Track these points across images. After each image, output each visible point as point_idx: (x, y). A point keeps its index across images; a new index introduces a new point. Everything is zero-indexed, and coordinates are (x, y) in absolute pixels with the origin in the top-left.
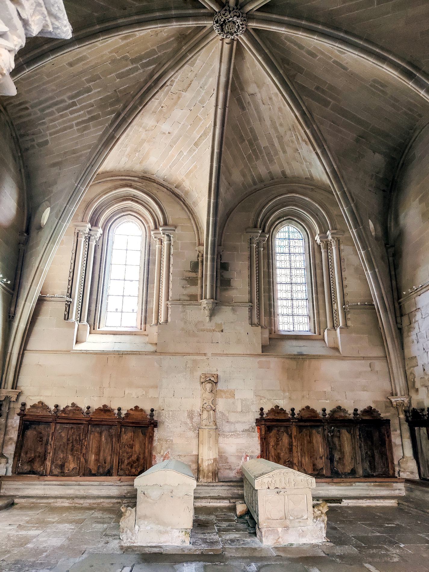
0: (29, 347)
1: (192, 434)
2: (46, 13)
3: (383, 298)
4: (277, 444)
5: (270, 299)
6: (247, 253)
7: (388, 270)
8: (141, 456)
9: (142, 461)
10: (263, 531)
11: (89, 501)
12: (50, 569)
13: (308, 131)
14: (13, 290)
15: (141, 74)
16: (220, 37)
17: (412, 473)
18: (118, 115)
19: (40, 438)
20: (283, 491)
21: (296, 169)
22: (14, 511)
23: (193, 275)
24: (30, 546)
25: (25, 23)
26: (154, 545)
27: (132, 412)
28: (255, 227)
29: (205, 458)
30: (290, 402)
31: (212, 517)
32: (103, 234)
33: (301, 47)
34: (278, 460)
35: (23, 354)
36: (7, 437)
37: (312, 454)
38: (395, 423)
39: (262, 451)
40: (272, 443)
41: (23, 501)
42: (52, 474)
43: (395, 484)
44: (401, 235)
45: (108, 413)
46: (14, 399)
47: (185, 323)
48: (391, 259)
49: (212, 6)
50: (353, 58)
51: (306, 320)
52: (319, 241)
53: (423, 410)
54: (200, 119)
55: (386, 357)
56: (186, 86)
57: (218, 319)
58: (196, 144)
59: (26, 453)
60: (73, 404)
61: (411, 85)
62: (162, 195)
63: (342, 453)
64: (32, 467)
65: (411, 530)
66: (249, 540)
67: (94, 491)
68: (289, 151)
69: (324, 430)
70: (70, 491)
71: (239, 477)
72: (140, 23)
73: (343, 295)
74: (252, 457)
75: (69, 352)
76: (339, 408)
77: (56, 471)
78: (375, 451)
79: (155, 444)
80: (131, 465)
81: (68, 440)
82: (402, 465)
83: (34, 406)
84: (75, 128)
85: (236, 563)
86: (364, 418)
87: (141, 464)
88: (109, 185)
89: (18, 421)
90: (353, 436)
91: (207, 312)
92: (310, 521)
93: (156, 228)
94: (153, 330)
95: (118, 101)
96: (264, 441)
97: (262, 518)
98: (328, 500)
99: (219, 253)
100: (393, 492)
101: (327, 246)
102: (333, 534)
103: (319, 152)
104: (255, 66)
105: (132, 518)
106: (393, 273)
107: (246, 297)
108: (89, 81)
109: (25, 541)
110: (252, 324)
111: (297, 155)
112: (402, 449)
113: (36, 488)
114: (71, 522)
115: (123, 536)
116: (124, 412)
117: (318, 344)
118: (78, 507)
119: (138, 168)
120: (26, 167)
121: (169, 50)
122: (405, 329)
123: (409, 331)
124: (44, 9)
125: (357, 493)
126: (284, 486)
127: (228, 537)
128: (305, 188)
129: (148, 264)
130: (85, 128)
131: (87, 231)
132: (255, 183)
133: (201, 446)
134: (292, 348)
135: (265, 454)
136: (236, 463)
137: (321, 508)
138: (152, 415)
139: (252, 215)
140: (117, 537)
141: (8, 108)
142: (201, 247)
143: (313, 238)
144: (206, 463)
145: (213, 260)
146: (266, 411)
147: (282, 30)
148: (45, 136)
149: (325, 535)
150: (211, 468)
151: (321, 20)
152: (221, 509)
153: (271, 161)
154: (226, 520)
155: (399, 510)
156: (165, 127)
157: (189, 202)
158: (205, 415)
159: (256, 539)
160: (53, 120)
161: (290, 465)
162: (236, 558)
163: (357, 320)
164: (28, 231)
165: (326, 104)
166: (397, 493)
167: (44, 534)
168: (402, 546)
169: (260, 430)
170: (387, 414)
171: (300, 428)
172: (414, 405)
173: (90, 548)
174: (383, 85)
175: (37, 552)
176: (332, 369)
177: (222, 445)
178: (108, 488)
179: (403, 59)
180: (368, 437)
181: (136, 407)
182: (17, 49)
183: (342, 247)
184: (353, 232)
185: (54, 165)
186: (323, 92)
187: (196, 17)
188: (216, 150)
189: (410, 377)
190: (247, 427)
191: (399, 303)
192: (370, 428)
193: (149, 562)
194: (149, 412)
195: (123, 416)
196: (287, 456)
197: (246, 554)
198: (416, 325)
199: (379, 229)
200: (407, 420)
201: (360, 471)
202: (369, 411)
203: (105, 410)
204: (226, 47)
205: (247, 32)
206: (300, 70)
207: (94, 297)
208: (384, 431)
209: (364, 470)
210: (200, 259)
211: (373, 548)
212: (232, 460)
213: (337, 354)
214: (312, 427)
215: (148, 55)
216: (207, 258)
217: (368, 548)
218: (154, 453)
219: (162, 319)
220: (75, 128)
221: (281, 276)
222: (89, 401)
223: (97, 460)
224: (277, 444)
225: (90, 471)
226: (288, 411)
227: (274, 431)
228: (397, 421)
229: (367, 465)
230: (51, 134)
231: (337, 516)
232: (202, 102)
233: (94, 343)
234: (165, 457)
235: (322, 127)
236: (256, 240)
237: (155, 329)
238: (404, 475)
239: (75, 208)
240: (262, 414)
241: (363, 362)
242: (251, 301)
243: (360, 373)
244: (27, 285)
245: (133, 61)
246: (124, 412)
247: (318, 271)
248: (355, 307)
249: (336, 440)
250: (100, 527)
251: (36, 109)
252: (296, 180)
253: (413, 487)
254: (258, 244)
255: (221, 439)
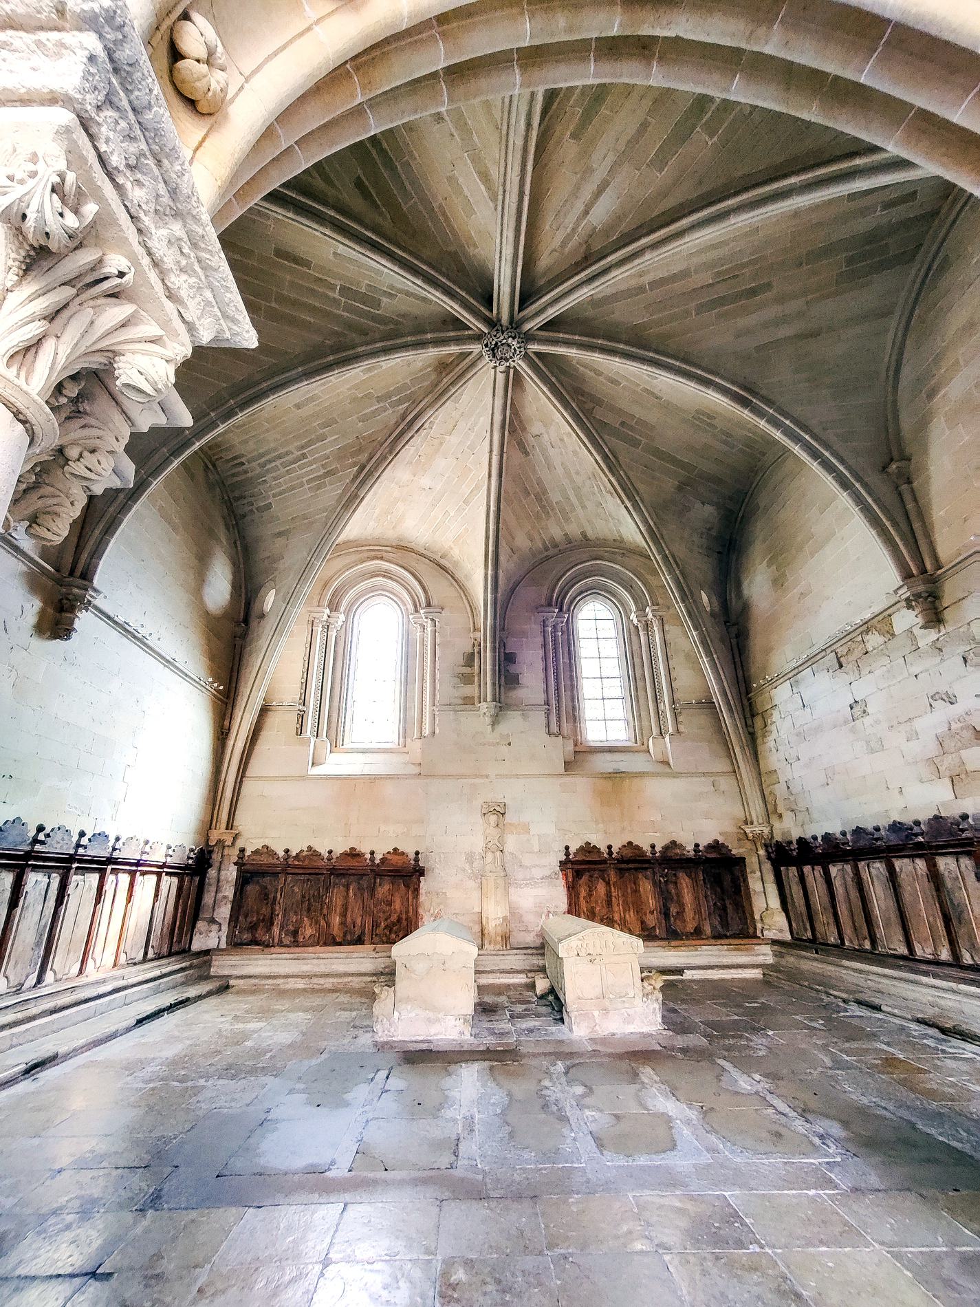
0: (247, 774)
1: (471, 884)
2: (219, 314)
3: (724, 691)
4: (590, 895)
5: (573, 700)
6: (540, 640)
7: (730, 657)
8: (404, 916)
9: (405, 923)
10: (573, 1015)
11: (331, 980)
12: (276, 1076)
13: (613, 479)
14: (228, 697)
15: (390, 415)
16: (492, 364)
17: (781, 931)
18: (363, 468)
19: (265, 896)
20: (598, 958)
21: (600, 528)
22: (228, 997)
23: (468, 670)
24: (249, 1044)
25: (191, 328)
26: (421, 1038)
27: (389, 857)
28: (550, 604)
29: (492, 916)
30: (607, 837)
31: (503, 999)
32: (346, 622)
33: (599, 373)
34: (592, 916)
35: (241, 782)
36: (220, 895)
37: (639, 908)
38: (752, 862)
39: (570, 905)
40: (583, 894)
41: (241, 982)
42: (281, 944)
43: (757, 947)
44: (745, 608)
45: (358, 859)
46: (229, 843)
47: (458, 735)
48: (734, 641)
49: (480, 326)
50: (667, 384)
51: (622, 725)
52: (635, 621)
53: (790, 843)
54: (470, 470)
55: (735, 772)
56: (451, 427)
57: (503, 728)
58: (466, 502)
59: (246, 917)
60: (310, 848)
61: (746, 414)
62: (423, 568)
63: (681, 905)
64: (253, 936)
65: (783, 1012)
66: (553, 1029)
67: (340, 967)
68: (589, 505)
69: (654, 874)
70: (305, 967)
71: (538, 942)
72: (386, 351)
73: (672, 691)
74: (555, 913)
75: (303, 778)
76: (674, 842)
77: (287, 940)
78: (727, 902)
79: (422, 898)
80: (390, 928)
81: (303, 897)
82: (766, 921)
83: (256, 852)
84: (306, 487)
85: (534, 1062)
86: (709, 856)
87: (403, 926)
88: (354, 558)
89: (235, 873)
90: (695, 880)
91: (488, 720)
92: (638, 1001)
93: (417, 611)
94: (416, 746)
95: (360, 450)
96: (572, 889)
97: (570, 997)
98: (664, 971)
99: (501, 640)
100: (755, 958)
101: (647, 626)
102: (674, 1021)
103: (629, 505)
104: (540, 402)
105: (390, 1002)
106: (737, 660)
107: (541, 698)
108: (325, 425)
109: (245, 1036)
110: (549, 734)
111: (600, 510)
112: (764, 898)
113: (258, 964)
114: (305, 1011)
115: (378, 1028)
116: (378, 857)
117: (641, 757)
118: (318, 990)
119: (391, 535)
120: (243, 538)
121: (426, 383)
122: (759, 733)
123: (764, 736)
124: (216, 309)
125: (707, 961)
126: (599, 951)
127: (524, 1026)
128: (613, 553)
129: (407, 657)
130: (319, 487)
131: (325, 617)
132: (547, 549)
133: (485, 900)
134: (605, 763)
135: (574, 909)
136: (535, 923)
137: (653, 982)
138: (417, 860)
139: (545, 591)
140: (370, 1029)
141: (219, 464)
142: (477, 634)
143: (628, 617)
144: (493, 925)
145: (494, 649)
146: (572, 850)
147: (572, 352)
148: (267, 498)
149: (660, 1020)
150: (499, 930)
151: (624, 337)
152: (515, 986)
153: (567, 520)
154: (521, 1002)
155: (766, 982)
156: (425, 481)
157: (458, 575)
158: (490, 856)
159: (564, 1028)
160: (275, 479)
161: (609, 922)
162: (535, 1055)
163: (695, 723)
164: (246, 620)
165: (635, 443)
166: (760, 960)
167: (268, 1027)
168: (770, 1033)
169: (566, 875)
170: (741, 850)
171: (621, 872)
172: (778, 837)
173: (332, 1045)
174: (711, 417)
175: (259, 1053)
176: (661, 791)
177: (514, 898)
178: (356, 961)
179: (733, 383)
180: (715, 881)
181: (395, 849)
182: (180, 359)
183: (667, 628)
184: (680, 608)
185: (280, 534)
186: (632, 428)
187: (458, 341)
188: (493, 508)
189: (770, 799)
190: (548, 873)
191: (749, 699)
192: (719, 870)
193: (413, 1063)
194: (412, 856)
195: (377, 862)
196: (605, 910)
197: (550, 1049)
198: (773, 728)
199: (716, 604)
200: (769, 858)
201: (708, 930)
202: (715, 846)
203: (353, 854)
204: (501, 378)
205: (526, 357)
206: (598, 402)
207: (336, 704)
208: (738, 873)
209: (713, 927)
210: (476, 649)
211: (729, 1037)
212: (529, 918)
213: (668, 770)
214: (636, 869)
215: (398, 390)
216: (485, 647)
217: (723, 1037)
218: (421, 911)
219: (427, 731)
220: (306, 487)
221: (587, 668)
222: (331, 842)
223: (343, 923)
224: (590, 895)
225: (334, 938)
226: (604, 849)
227: (585, 878)
228: (755, 860)
229: (716, 922)
230: (274, 496)
231: (675, 991)
232: (472, 447)
233: (336, 764)
234: (436, 917)
235: (631, 474)
236: (551, 622)
237: (418, 744)
238: (769, 934)
239: (308, 589)
240: (567, 854)
241: (703, 779)
242: (547, 703)
243: (701, 793)
244: (245, 691)
245: (379, 399)
246: (378, 857)
247: (637, 660)
248: (689, 706)
249: (671, 886)
250: (346, 1016)
251: (254, 464)
252: (602, 543)
253: (783, 950)
254: (554, 627)
255: (512, 890)
